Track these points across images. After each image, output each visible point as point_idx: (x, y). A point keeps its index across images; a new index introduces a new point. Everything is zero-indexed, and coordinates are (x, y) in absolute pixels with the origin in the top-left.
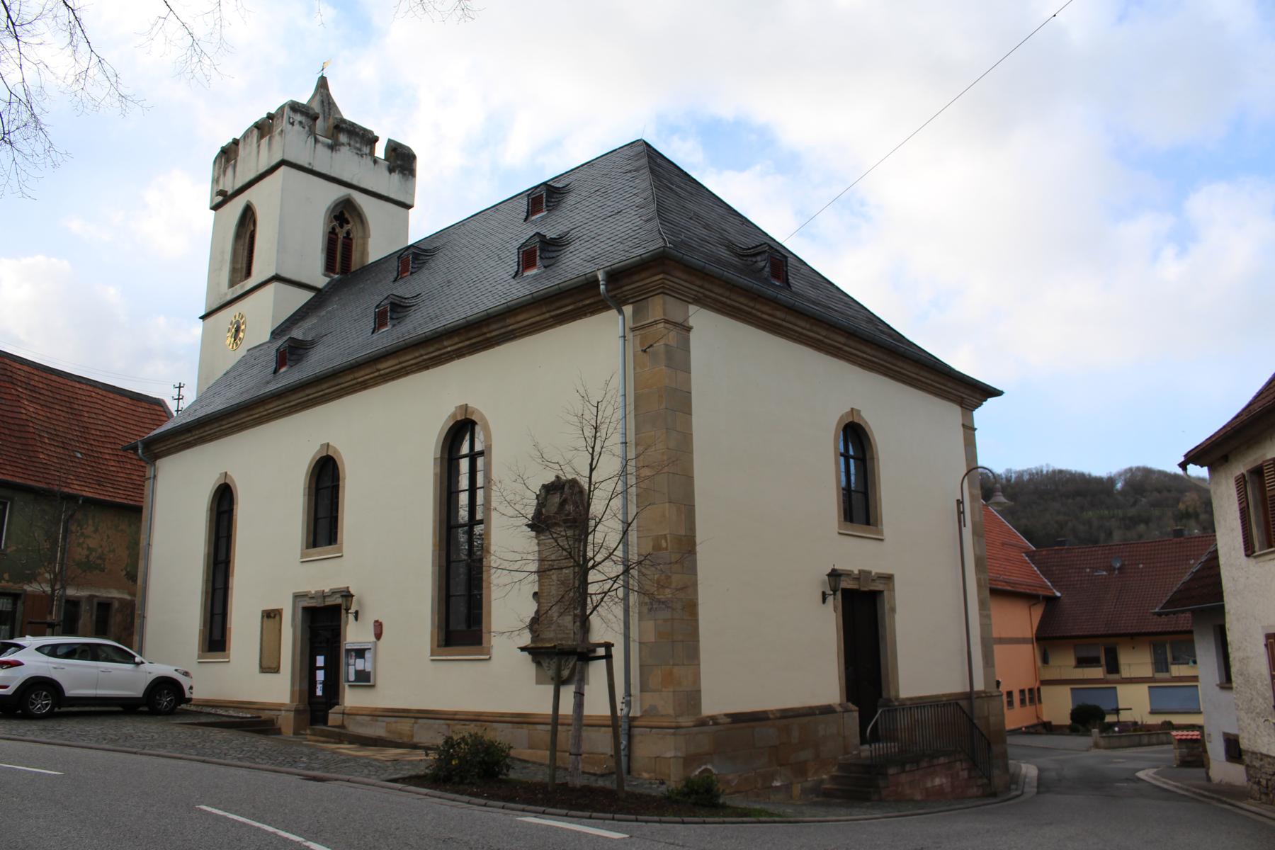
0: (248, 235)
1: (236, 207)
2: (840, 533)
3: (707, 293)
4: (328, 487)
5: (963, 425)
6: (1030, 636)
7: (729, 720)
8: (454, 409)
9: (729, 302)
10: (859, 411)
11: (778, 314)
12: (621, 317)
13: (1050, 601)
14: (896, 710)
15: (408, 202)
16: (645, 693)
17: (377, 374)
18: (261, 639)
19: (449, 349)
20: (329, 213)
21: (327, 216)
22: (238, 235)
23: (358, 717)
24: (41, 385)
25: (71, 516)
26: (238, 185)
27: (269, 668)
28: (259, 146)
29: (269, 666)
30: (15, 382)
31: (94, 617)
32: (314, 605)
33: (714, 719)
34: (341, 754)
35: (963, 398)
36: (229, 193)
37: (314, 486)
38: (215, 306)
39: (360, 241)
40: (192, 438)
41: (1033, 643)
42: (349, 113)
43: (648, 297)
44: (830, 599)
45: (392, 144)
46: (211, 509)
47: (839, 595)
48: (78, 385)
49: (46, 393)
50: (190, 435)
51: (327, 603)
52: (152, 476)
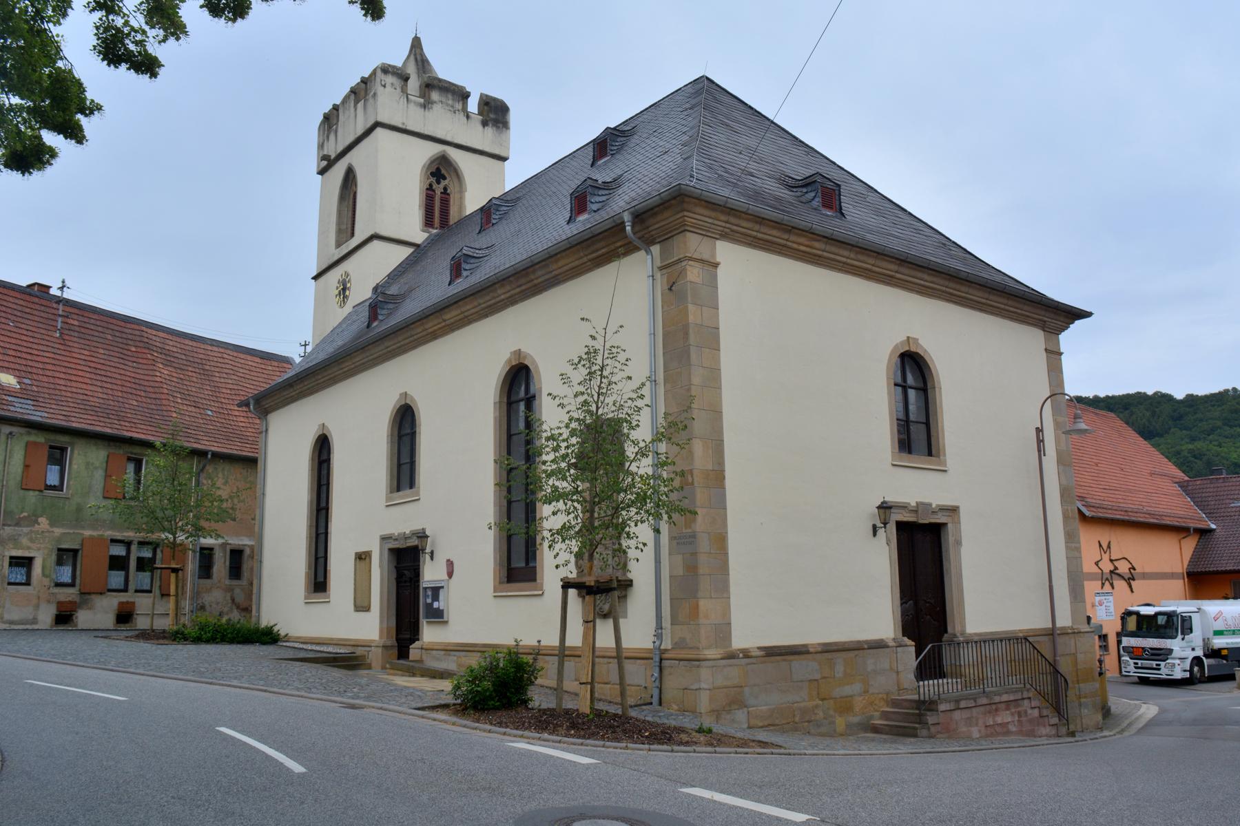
0: (352, 196)
1: (339, 171)
2: (894, 465)
3: (735, 228)
4: (408, 434)
5: (1046, 350)
6: (1181, 571)
7: (762, 653)
8: (509, 355)
9: (760, 235)
10: (916, 340)
11: (816, 244)
12: (649, 257)
13: (1204, 533)
14: (959, 644)
15: (503, 154)
16: (677, 627)
17: (443, 324)
18: (355, 580)
19: (503, 297)
20: (425, 169)
21: (423, 174)
22: (342, 197)
23: (434, 652)
24: (175, 350)
25: (202, 470)
26: (340, 148)
27: (362, 607)
28: (356, 110)
29: (362, 606)
30: (151, 347)
31: (228, 563)
32: (397, 546)
33: (746, 654)
34: (396, 685)
35: (1045, 322)
36: (332, 157)
37: (396, 433)
38: (324, 267)
39: (457, 196)
40: (294, 393)
41: (1184, 579)
42: (444, 69)
43: (672, 236)
44: (881, 532)
45: (485, 98)
46: (313, 459)
47: (892, 528)
48: (210, 348)
49: (180, 356)
50: (291, 390)
51: (408, 545)
52: (264, 429)
